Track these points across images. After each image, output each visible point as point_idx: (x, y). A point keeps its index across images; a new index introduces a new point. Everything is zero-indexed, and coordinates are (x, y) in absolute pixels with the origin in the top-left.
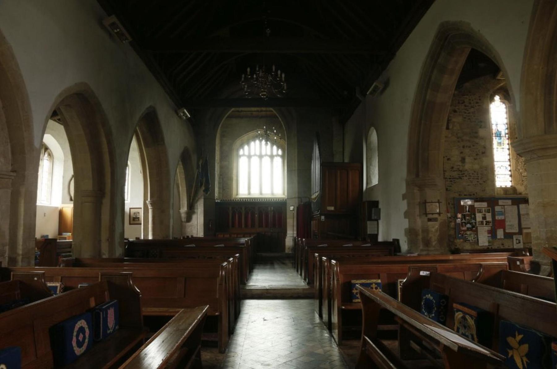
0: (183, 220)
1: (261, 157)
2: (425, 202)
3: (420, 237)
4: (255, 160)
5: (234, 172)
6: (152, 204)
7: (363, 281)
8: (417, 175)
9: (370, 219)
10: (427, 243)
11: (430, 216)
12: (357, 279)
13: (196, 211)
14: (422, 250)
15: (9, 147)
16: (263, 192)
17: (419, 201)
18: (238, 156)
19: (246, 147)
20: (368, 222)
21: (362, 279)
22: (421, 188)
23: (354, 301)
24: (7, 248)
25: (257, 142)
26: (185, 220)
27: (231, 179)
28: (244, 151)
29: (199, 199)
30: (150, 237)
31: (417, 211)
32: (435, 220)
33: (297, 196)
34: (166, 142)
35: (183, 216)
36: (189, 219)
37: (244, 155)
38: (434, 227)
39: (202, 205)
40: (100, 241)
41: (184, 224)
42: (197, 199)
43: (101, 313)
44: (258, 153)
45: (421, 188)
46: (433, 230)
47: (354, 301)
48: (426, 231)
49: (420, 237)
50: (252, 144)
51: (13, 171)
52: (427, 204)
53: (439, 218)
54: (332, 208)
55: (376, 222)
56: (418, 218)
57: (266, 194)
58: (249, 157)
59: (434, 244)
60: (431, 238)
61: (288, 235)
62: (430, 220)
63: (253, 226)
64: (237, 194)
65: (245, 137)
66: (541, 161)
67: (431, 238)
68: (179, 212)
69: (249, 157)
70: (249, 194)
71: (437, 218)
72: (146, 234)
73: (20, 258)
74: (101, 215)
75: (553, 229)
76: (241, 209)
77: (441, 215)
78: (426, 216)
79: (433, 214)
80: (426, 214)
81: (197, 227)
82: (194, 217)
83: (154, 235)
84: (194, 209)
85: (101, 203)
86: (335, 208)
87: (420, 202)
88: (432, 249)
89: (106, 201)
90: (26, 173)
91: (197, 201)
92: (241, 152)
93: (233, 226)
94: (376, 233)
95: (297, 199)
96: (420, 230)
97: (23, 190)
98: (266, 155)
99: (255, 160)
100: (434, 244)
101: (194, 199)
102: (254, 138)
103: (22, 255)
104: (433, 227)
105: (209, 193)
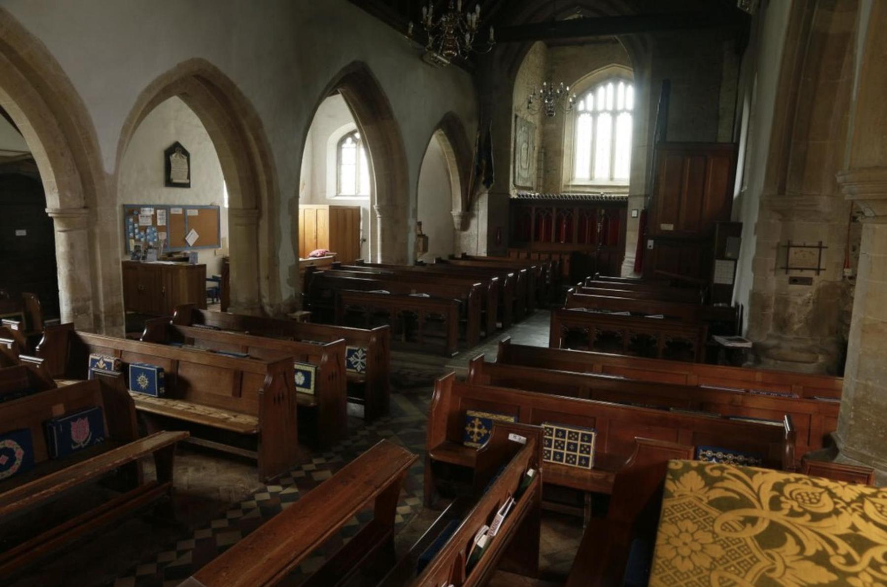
0: (456, 227)
1: (615, 113)
2: (789, 246)
3: (771, 311)
4: (604, 120)
5: (566, 140)
6: (381, 210)
7: (486, 415)
8: (782, 190)
9: (723, 257)
10: (783, 324)
11: (796, 274)
12: (477, 410)
13: (476, 213)
14: (770, 336)
15: (77, 176)
16: (617, 176)
17: (778, 240)
18: (577, 114)
19: (590, 97)
21: (484, 411)
22: (785, 215)
23: (465, 444)
24: (90, 303)
25: (610, 86)
27: (559, 154)
28: (587, 103)
29: (481, 194)
30: (379, 262)
31: (772, 260)
32: (808, 281)
33: (643, 193)
34: (396, 114)
35: (457, 220)
36: (465, 225)
38: (802, 297)
39: (486, 203)
40: (259, 279)
41: (458, 232)
42: (478, 193)
43: (54, 428)
44: (610, 108)
45: (785, 215)
46: (799, 301)
47: (465, 444)
48: (783, 301)
49: (771, 311)
50: (601, 90)
51: (85, 207)
52: (792, 250)
53: (816, 279)
55: (732, 263)
56: (773, 273)
57: (620, 180)
58: (595, 114)
60: (791, 315)
61: (626, 259)
62: (794, 281)
64: (572, 179)
67: (791, 315)
68: (451, 215)
69: (595, 114)
72: (374, 256)
73: (103, 316)
74: (258, 243)
75: (870, 383)
76: (551, 210)
77: (821, 273)
78: (787, 273)
79: (802, 269)
80: (787, 269)
82: (474, 222)
83: (383, 257)
84: (473, 210)
85: (258, 226)
87: (779, 244)
88: (790, 336)
89: (264, 224)
90: (98, 209)
91: (478, 197)
92: (581, 106)
93: (537, 238)
94: (730, 283)
95: (642, 199)
96: (773, 298)
97: (97, 230)
98: (624, 110)
99: (604, 120)
100: (796, 327)
102: (604, 80)
104: (800, 295)
105: (491, 186)
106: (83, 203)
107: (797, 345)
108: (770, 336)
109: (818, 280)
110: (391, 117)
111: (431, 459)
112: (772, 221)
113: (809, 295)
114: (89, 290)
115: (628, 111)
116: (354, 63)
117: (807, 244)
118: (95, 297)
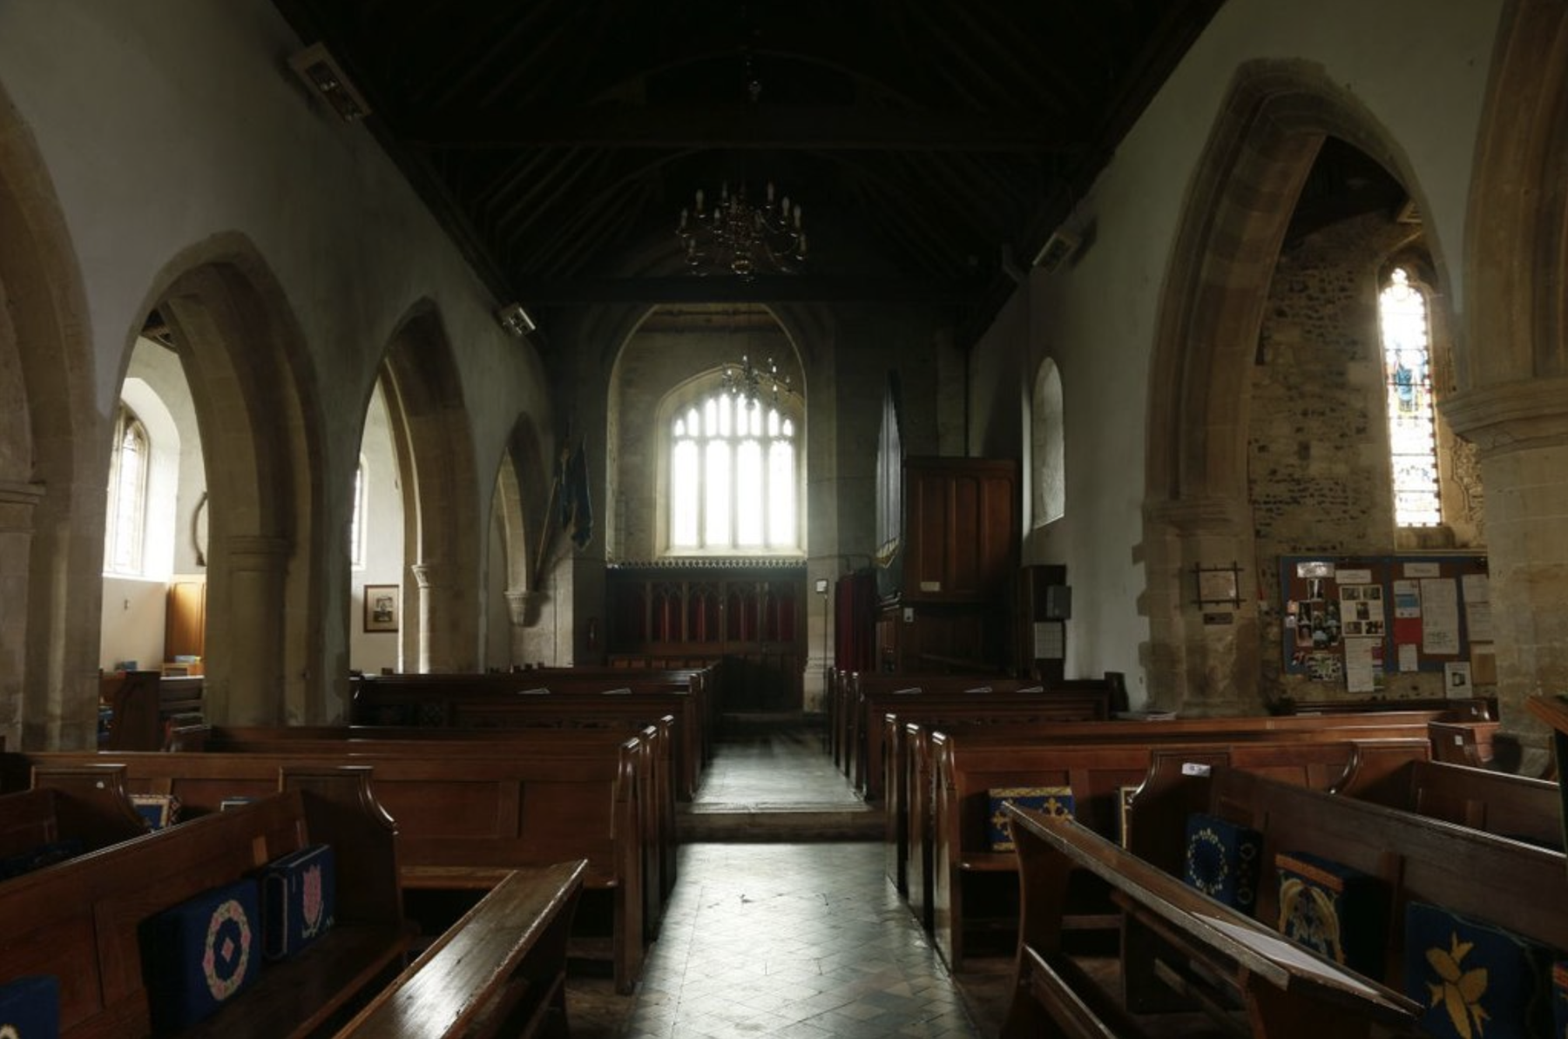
0: (515, 620)
1: (734, 441)
2: (1197, 570)
3: (1183, 668)
4: (718, 451)
6: (429, 574)
7: (1023, 791)
8: (1175, 494)
9: (1042, 617)
10: (1202, 684)
11: (1210, 609)
12: (1005, 786)
13: (551, 593)
14: (1188, 705)
16: (742, 541)
17: (1179, 565)
18: (671, 440)
19: (693, 415)
20: (1036, 626)
23: (996, 847)
25: (725, 399)
26: (522, 619)
27: (650, 504)
28: (688, 425)
29: (560, 560)
30: (423, 669)
32: (1226, 619)
33: (835, 551)
35: (516, 607)
36: (532, 616)
37: (686, 437)
38: (1222, 639)
41: (518, 629)
42: (554, 559)
44: (726, 431)
46: (1220, 647)
48: (1199, 650)
49: (1183, 668)
50: (710, 404)
51: (35, 482)
52: (1202, 575)
53: (1236, 614)
54: (935, 587)
57: (750, 547)
58: (702, 441)
59: (1221, 686)
60: (1213, 669)
61: (811, 663)
62: (1209, 619)
63: (712, 635)
64: (668, 547)
65: (690, 386)
66: (1522, 453)
67: (1213, 669)
69: (702, 441)
70: (702, 545)
71: (1230, 615)
72: (411, 657)
73: (55, 728)
75: (1557, 644)
76: (680, 587)
77: (1243, 605)
79: (1218, 602)
80: (1199, 603)
81: (554, 639)
82: (547, 611)
83: (432, 660)
84: (546, 588)
85: (284, 572)
86: (943, 586)
87: (1181, 570)
88: (1217, 700)
89: (300, 569)
90: (74, 486)
92: (679, 428)
94: (1058, 655)
96: (1184, 648)
98: (749, 437)
99: (718, 451)
101: (545, 561)
102: (715, 390)
103: (63, 718)
104: (1220, 640)
105: (587, 543)
106: (28, 473)
107: (1229, 712)
108: (1188, 705)
109: (1240, 616)
110: (462, 404)
111: (964, 871)
112: (1168, 538)
113: (1230, 638)
114: (21, 668)
115: (754, 438)
116: (424, 300)
117: (1418, 495)
118: (37, 685)
